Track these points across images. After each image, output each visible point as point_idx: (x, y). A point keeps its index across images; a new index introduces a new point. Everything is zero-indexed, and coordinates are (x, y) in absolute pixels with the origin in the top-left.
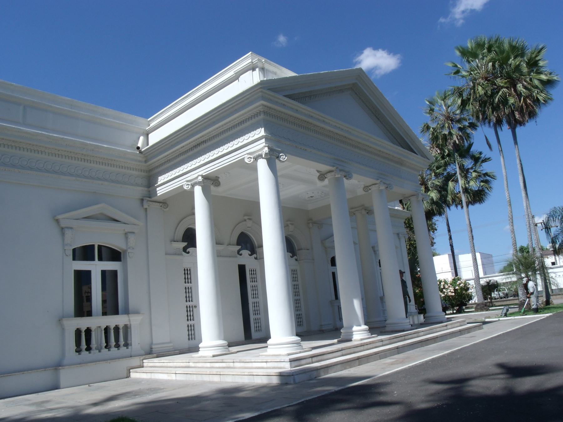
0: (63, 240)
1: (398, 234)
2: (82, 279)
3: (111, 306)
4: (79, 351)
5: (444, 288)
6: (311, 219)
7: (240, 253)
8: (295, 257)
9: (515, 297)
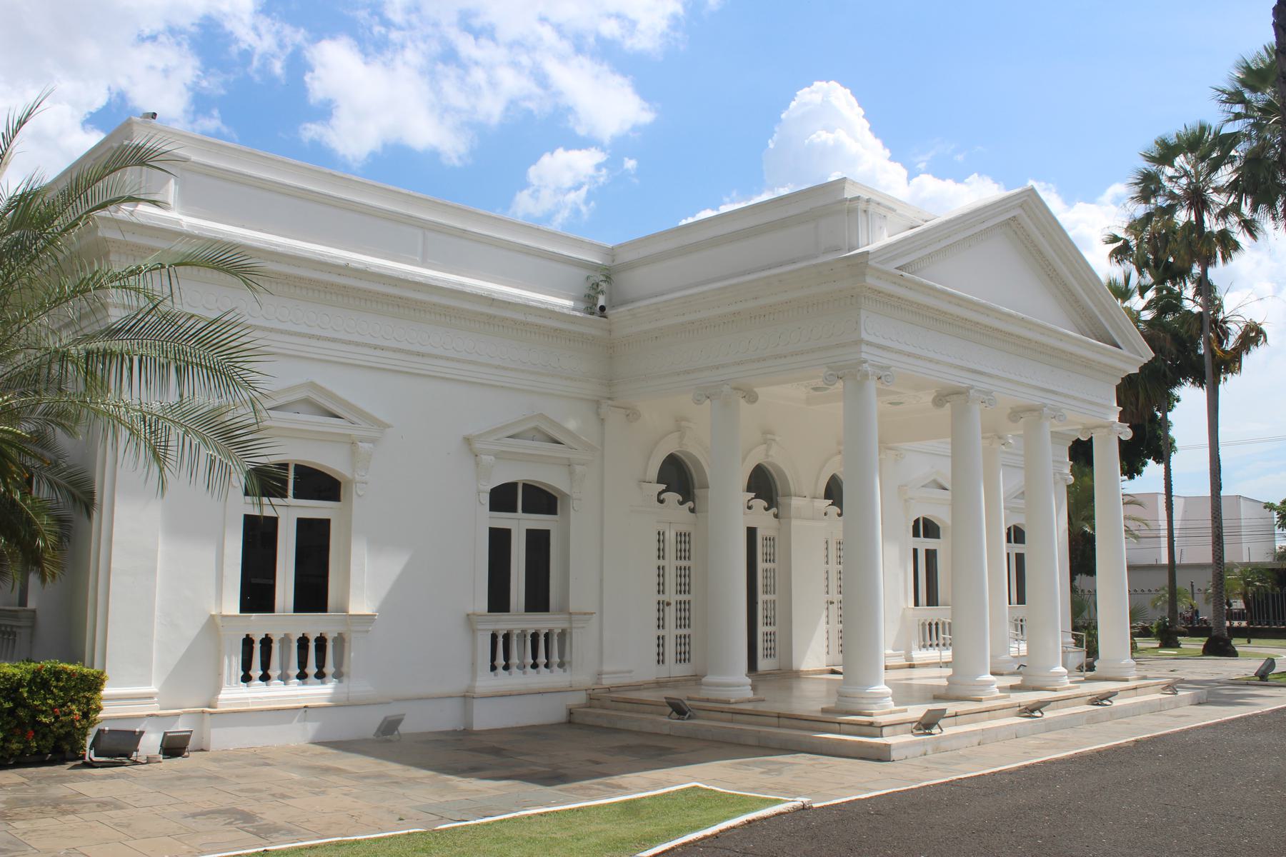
7: (663, 496)
8: (774, 510)
9: (107, 355)
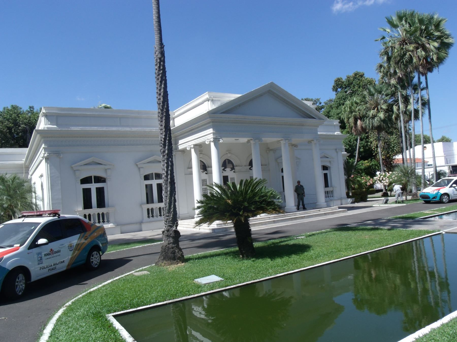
0: (140, 173)
1: (336, 149)
2: (87, 192)
3: (101, 203)
4: (149, 217)
5: (383, 180)
6: (269, 148)
